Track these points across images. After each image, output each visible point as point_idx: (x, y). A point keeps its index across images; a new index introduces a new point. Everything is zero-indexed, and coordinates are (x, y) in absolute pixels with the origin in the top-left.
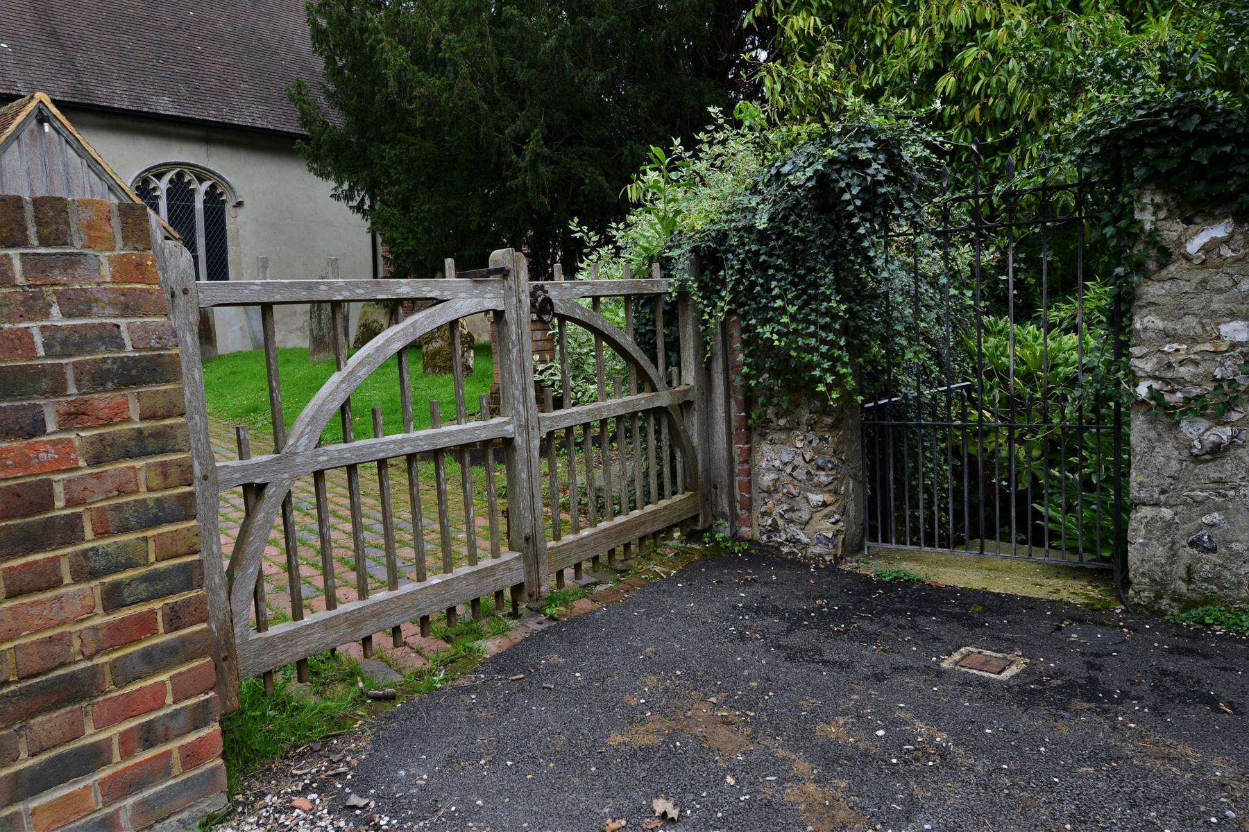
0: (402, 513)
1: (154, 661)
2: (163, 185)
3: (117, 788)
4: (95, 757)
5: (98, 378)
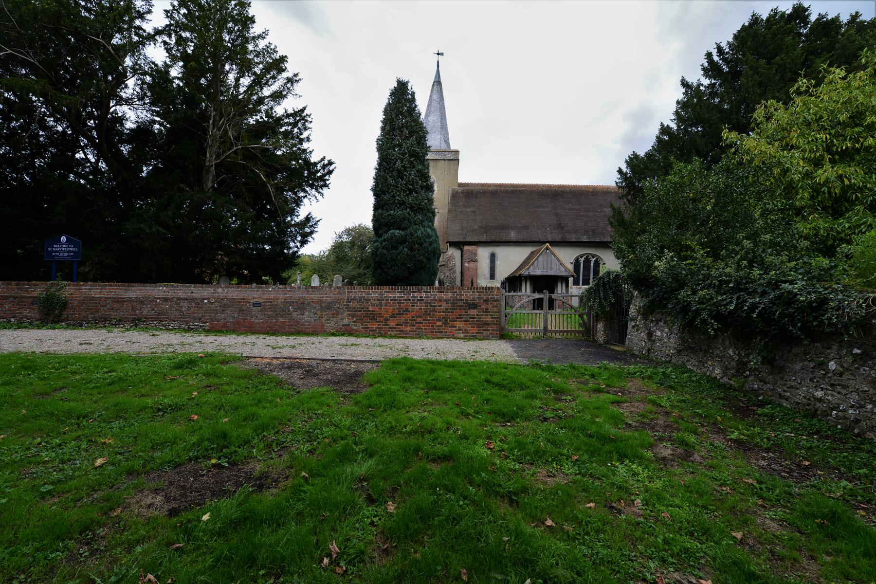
0: (561, 321)
1: (494, 324)
2: (582, 260)
3: (490, 334)
4: (489, 330)
5: (493, 301)
